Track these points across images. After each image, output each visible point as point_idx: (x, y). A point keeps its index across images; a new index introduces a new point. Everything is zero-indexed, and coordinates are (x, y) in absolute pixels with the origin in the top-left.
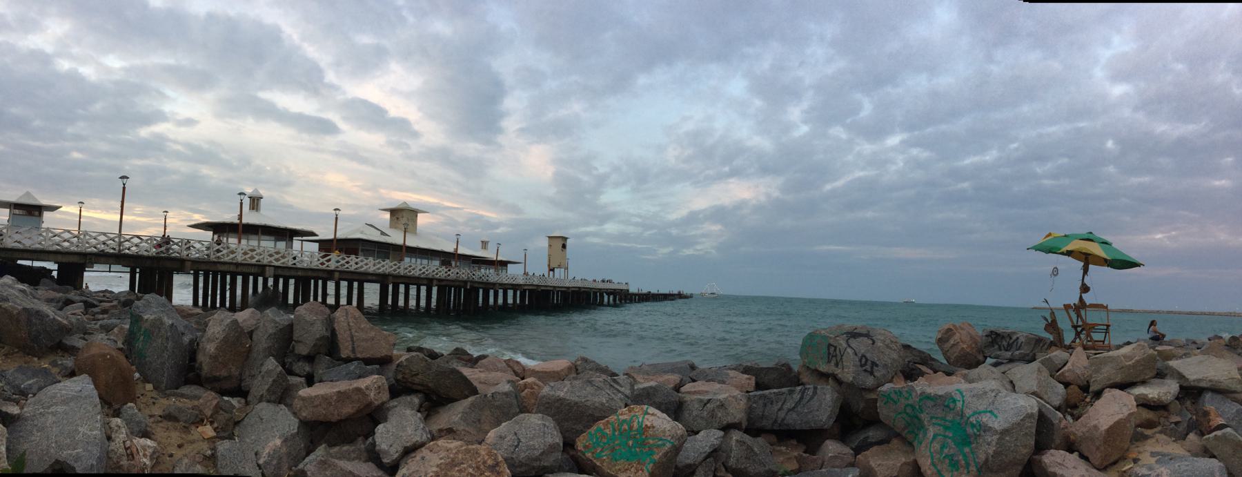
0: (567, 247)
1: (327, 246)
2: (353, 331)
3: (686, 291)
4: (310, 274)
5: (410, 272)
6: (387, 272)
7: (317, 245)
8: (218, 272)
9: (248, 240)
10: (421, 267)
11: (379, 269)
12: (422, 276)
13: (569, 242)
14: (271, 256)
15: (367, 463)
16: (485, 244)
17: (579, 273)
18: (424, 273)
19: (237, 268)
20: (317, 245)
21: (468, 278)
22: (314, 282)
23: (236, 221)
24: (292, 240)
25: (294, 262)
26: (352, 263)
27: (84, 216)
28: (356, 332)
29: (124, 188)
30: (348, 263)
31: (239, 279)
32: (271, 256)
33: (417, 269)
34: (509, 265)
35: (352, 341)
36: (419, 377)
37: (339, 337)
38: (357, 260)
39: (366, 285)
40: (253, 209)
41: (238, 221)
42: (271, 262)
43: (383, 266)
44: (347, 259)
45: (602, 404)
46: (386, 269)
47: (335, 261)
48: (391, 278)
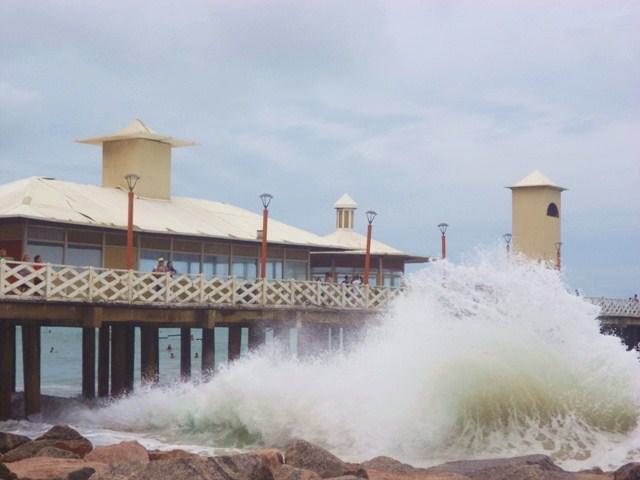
0: (563, 209)
4: (130, 317)
5: (217, 297)
9: (229, 262)
10: (209, 284)
11: (69, 290)
13: (565, 205)
16: (344, 216)
18: (184, 296)
21: (297, 303)
26: (48, 282)
27: (255, 211)
29: (444, 238)
30: (158, 288)
33: (201, 290)
43: (79, 284)
46: (88, 290)
48: (98, 311)
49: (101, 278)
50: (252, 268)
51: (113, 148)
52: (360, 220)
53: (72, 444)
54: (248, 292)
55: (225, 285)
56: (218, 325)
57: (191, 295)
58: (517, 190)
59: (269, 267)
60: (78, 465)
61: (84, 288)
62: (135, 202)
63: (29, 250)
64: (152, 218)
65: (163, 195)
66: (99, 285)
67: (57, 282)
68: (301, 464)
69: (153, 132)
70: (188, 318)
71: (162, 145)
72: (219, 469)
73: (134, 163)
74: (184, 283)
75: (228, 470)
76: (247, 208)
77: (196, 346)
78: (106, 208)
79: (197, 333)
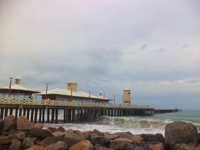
0: (131, 93)
1: (44, 97)
4: (71, 108)
7: (42, 96)
14: (22, 101)
15: (198, 147)
16: (101, 94)
20: (42, 96)
23: (9, 88)
27: (88, 93)
28: (24, 123)
30: (51, 103)
32: (22, 101)
35: (22, 125)
37: (18, 124)
38: (55, 102)
39: (59, 110)
40: (17, 83)
41: (9, 88)
44: (69, 103)
45: (79, 139)
47: (47, 102)
48: (66, 107)
51: (69, 84)
52: (103, 95)
56: (83, 109)
63: (57, 98)
64: (74, 94)
65: (76, 91)
66: (67, 104)
68: (95, 133)
69: (75, 82)
70: (79, 108)
71: (76, 84)
73: (72, 87)
74: (78, 103)
75: (85, 135)
78: (68, 93)
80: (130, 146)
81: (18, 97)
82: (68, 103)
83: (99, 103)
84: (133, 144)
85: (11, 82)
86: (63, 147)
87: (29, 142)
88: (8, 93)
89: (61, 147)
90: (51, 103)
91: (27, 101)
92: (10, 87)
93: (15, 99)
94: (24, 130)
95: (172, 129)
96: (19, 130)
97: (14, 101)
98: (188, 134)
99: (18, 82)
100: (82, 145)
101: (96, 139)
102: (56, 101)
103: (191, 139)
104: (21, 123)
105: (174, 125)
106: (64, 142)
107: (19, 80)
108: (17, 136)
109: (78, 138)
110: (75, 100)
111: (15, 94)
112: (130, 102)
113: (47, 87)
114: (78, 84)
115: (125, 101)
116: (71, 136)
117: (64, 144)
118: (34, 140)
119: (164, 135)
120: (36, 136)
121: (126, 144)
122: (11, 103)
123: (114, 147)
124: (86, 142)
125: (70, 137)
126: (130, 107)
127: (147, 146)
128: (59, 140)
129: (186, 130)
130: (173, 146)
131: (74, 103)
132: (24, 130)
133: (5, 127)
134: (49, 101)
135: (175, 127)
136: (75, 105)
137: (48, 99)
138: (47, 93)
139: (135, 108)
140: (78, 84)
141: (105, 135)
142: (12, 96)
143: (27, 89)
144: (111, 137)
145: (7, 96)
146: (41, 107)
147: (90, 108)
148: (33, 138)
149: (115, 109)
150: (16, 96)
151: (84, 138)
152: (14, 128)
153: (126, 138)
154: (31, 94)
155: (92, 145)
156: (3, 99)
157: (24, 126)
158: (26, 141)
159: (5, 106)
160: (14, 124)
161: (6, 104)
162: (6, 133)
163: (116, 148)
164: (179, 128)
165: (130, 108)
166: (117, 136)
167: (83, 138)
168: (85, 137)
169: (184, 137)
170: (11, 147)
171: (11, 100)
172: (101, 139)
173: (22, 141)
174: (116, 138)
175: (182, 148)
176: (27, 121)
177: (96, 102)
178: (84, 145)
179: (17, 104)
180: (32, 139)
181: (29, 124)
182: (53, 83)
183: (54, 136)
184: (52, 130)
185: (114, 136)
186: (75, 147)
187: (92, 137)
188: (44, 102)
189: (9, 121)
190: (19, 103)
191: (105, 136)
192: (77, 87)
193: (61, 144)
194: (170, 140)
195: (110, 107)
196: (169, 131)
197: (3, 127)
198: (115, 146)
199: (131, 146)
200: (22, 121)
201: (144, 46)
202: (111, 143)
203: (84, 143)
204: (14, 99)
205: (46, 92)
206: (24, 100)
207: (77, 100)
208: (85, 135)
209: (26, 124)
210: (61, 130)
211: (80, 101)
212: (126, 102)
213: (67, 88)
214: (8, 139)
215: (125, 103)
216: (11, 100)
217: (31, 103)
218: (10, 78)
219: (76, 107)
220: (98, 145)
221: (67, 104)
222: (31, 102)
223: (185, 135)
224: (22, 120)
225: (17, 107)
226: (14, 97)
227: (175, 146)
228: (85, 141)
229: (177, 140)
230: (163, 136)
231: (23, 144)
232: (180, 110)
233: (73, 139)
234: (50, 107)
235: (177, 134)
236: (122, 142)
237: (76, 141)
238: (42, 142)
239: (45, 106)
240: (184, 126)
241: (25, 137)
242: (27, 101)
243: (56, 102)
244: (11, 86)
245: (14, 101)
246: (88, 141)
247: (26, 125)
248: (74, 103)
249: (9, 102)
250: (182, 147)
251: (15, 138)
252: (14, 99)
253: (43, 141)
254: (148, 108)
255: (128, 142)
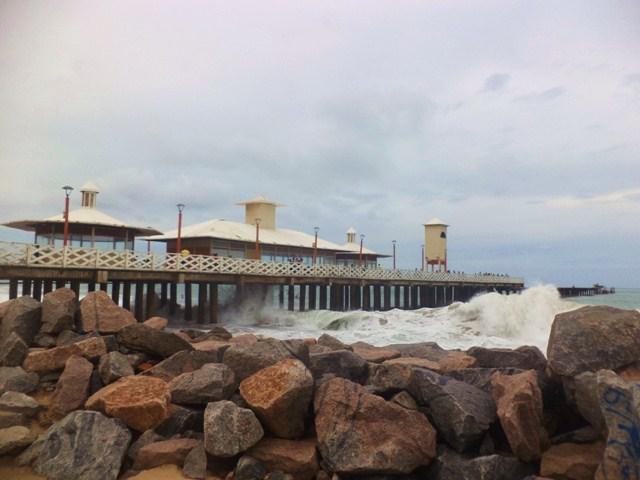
0: (448, 235)
1: (174, 246)
2: (99, 311)
3: (608, 286)
6: (239, 272)
7: (165, 244)
8: (53, 279)
9: (82, 241)
12: (279, 275)
14: (104, 258)
16: (351, 237)
17: (462, 267)
18: (280, 271)
19: (61, 273)
20: (165, 244)
22: (172, 286)
23: (63, 220)
24: (133, 240)
25: (37, 259)
26: (221, 265)
27: (312, 234)
31: (133, 288)
32: (104, 258)
34: (378, 259)
36: (139, 339)
38: (205, 260)
40: (87, 205)
42: (104, 265)
45: (271, 358)
47: (181, 261)
49: (244, 263)
50: (310, 259)
51: (250, 207)
52: (358, 239)
53: (223, 335)
54: (308, 270)
55: (269, 265)
56: (295, 284)
57: (284, 271)
58: (427, 226)
59: (318, 260)
60: (223, 344)
61: (93, 260)
62: (260, 231)
63: (213, 251)
64: (267, 238)
65: (271, 227)
66: (243, 266)
67: (225, 265)
68: (324, 344)
69: (268, 200)
70: (282, 281)
71: (271, 206)
72: (284, 346)
73: (259, 213)
74: (280, 266)
75: (289, 347)
76: (308, 233)
77: (286, 295)
78: (247, 233)
79: (169, 286)
80: (429, 378)
81: (92, 246)
82: (248, 264)
83: (346, 264)
84: (442, 374)
85: (67, 199)
86: (221, 379)
87: (117, 365)
88: (61, 236)
89: (214, 379)
90: (195, 263)
91: (119, 259)
92: (66, 216)
93: (84, 253)
94: (102, 334)
95: (569, 328)
96: (86, 333)
97: (82, 257)
98: (624, 344)
99: (92, 200)
100: (279, 373)
101: (325, 359)
102: (211, 257)
103: (632, 359)
104: (94, 312)
105: (579, 317)
106: (224, 367)
107: (92, 195)
108: (81, 347)
109: (267, 355)
110: (271, 255)
111: (84, 238)
112: (444, 263)
113: (180, 215)
114: (280, 205)
115: (431, 258)
116: (247, 348)
117: (223, 372)
118: (133, 363)
119: (544, 350)
120: (139, 348)
121: (416, 371)
122: (72, 264)
123: (380, 381)
124: (293, 364)
125: (241, 350)
126: (447, 278)
127: (487, 380)
128: (211, 361)
129: (618, 331)
130: (570, 378)
131: (265, 265)
132: (102, 334)
133: (46, 322)
134: (189, 259)
135: (579, 323)
136: (269, 271)
137: (186, 252)
138: (182, 235)
139: (461, 283)
140: (280, 205)
141: (355, 349)
142: (76, 244)
143: (119, 223)
144: (374, 355)
145: (59, 243)
146: (164, 277)
147: (318, 280)
148: (129, 356)
149: (396, 283)
150: (87, 245)
151: (288, 353)
152: (74, 327)
153: (422, 358)
154: (132, 239)
155: (309, 374)
156: (47, 252)
157: (102, 323)
158: (108, 361)
159: (56, 274)
160: (72, 315)
161: (59, 266)
162: (51, 340)
163: (387, 386)
164: (595, 326)
165: (447, 282)
166: (394, 352)
167: (283, 354)
168: (288, 349)
169: (610, 353)
170: (62, 378)
171: (72, 257)
172: (342, 359)
173: (95, 361)
174: (389, 359)
175: (599, 381)
176: (111, 306)
177: (337, 263)
178: (285, 373)
179: (90, 267)
180: (128, 359)
181: (117, 317)
182: (207, 206)
183: (194, 349)
184: (193, 338)
185: (382, 354)
186: (257, 379)
187: (311, 354)
188: (172, 262)
189: (56, 307)
190: (98, 266)
191: (356, 351)
192: (274, 215)
193: (216, 370)
194: (560, 362)
195: (378, 277)
196: (560, 332)
197: (40, 323)
198: (384, 379)
199: (434, 380)
200: (95, 307)
201: (496, 83)
202: (373, 372)
203: (284, 369)
204: (81, 253)
205: (177, 231)
206: (112, 255)
207: (274, 255)
208: (289, 347)
209: (109, 315)
210: (219, 336)
211: (286, 259)
212: (433, 262)
213: (244, 220)
214: (55, 355)
215: (430, 266)
216: (72, 257)
217: (133, 263)
218: (65, 188)
219: (274, 277)
220: (331, 375)
221: (243, 266)
222: (133, 260)
223: (613, 345)
224: (97, 302)
225: (91, 277)
226: (81, 245)
227: (578, 377)
228: (289, 361)
229: (586, 362)
230: (540, 353)
231: (100, 370)
232: (609, 290)
233: (251, 357)
234: (191, 278)
235: (586, 344)
236: (405, 368)
237: (261, 364)
238: (157, 366)
239: (177, 274)
240: (613, 318)
241: (103, 351)
242: (119, 259)
243: (211, 261)
244: (70, 214)
245: (80, 257)
246: (297, 362)
247: (110, 318)
248: (265, 265)
249: (66, 263)
250: (599, 379)
251: (74, 353)
252: (81, 253)
253: (162, 363)
254: (505, 281)
255: (424, 368)
